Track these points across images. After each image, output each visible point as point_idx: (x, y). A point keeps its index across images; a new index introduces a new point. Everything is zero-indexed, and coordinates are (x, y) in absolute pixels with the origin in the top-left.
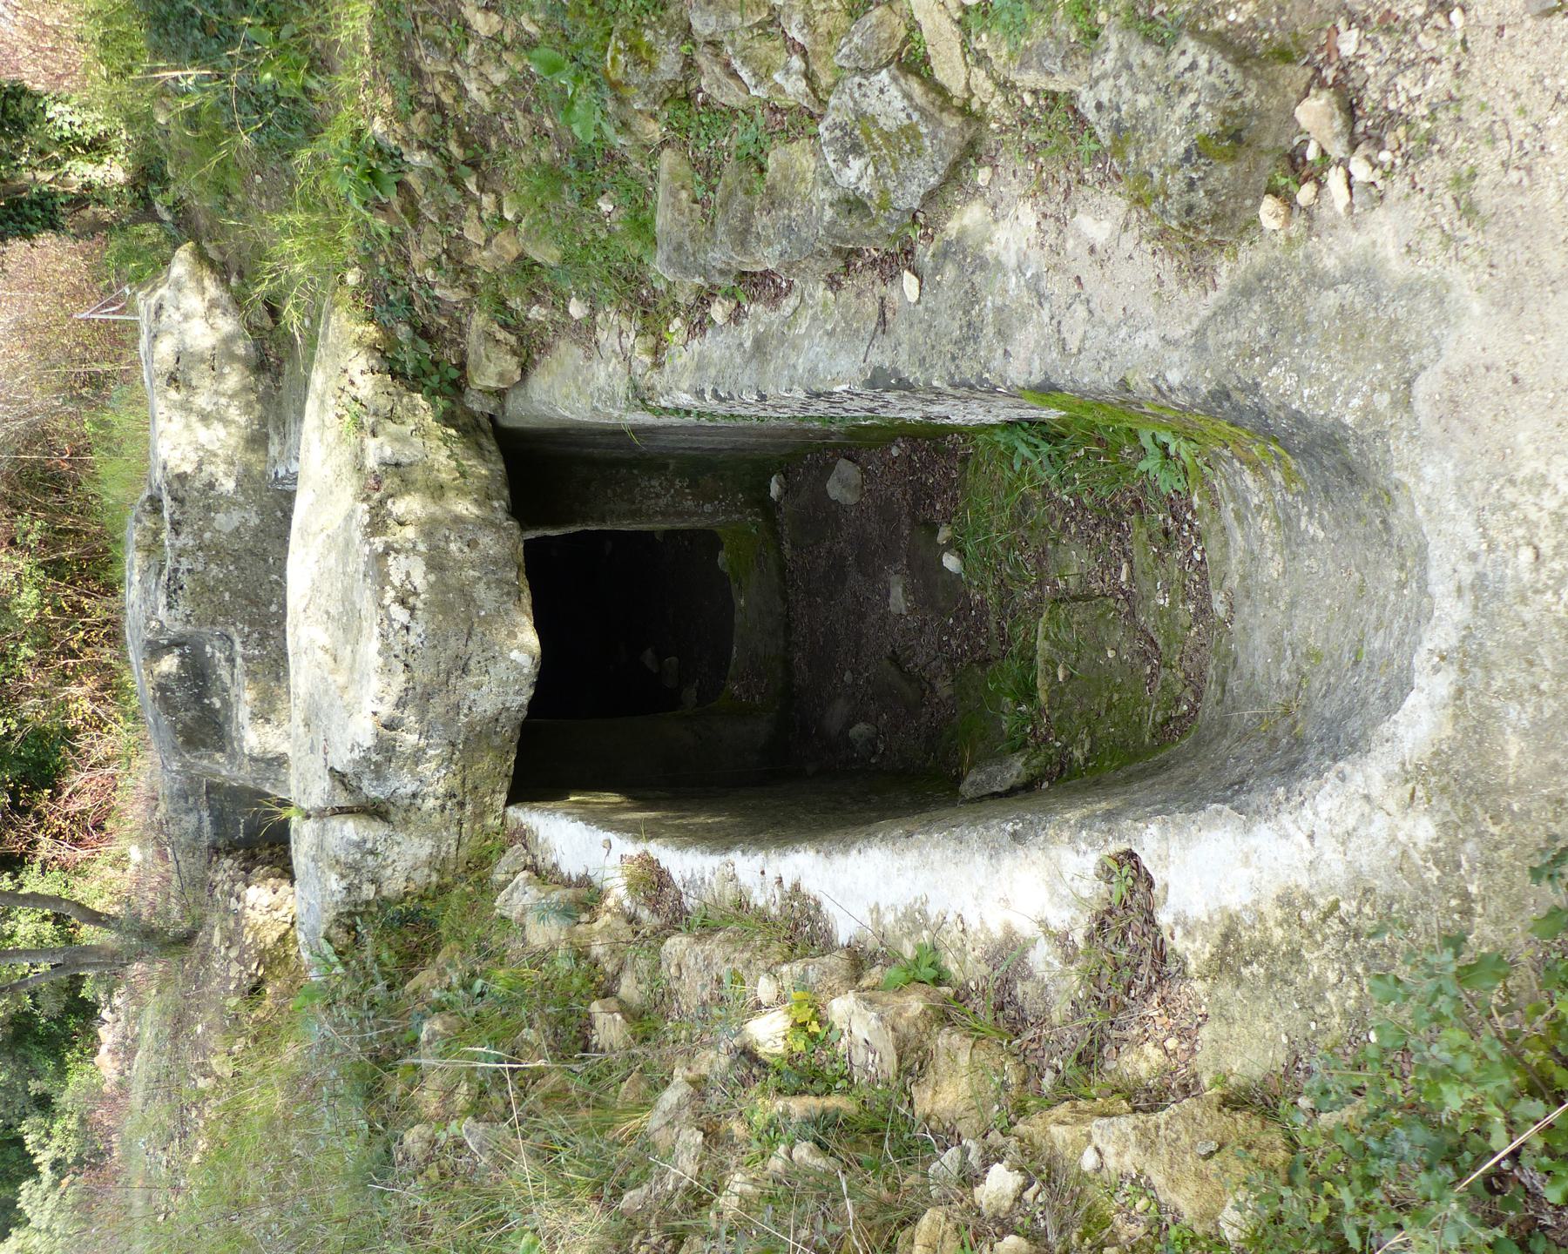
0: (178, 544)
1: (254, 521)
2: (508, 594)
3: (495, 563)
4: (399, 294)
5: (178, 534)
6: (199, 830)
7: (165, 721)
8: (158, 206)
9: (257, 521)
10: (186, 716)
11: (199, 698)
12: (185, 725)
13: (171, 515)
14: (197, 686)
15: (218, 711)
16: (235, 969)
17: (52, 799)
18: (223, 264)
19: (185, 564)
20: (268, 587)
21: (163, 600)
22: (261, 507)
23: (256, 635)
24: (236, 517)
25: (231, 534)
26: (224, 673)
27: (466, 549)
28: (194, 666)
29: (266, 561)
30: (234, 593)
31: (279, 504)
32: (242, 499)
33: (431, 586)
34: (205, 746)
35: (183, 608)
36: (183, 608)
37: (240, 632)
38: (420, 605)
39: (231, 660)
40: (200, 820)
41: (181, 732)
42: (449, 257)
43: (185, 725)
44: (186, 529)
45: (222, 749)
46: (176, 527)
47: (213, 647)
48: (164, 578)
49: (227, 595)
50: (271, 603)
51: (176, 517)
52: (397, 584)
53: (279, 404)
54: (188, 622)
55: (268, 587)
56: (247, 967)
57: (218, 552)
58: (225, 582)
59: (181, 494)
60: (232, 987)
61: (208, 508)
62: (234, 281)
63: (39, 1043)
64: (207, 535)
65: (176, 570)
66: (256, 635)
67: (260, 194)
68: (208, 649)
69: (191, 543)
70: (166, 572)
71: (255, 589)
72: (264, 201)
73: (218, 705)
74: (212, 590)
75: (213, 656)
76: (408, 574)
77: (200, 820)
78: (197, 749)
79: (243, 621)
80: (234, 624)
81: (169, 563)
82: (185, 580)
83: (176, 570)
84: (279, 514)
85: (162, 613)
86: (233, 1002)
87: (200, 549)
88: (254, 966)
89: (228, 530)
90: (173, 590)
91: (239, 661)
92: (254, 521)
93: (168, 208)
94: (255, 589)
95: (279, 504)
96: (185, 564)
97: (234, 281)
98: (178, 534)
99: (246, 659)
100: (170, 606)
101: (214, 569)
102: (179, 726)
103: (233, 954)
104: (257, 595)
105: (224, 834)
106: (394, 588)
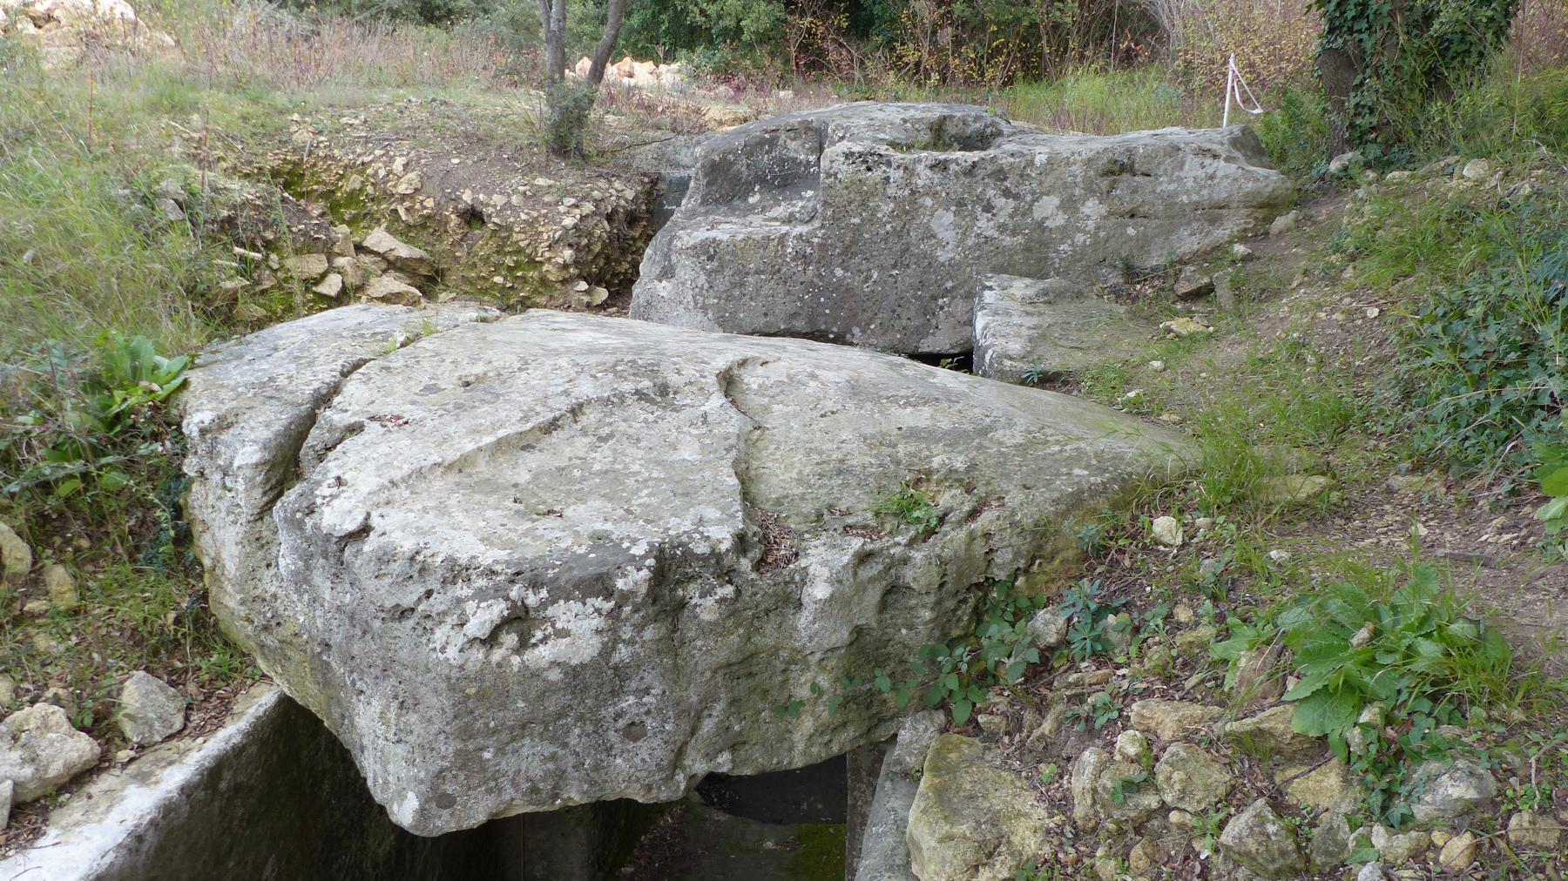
0: (920, 168)
1: (943, 256)
2: (534, 790)
3: (597, 768)
4: (1114, 637)
5: (932, 167)
6: (677, 165)
7: (739, 143)
8: (1350, 155)
9: (941, 259)
10: (741, 166)
11: (761, 180)
12: (731, 164)
13: (956, 161)
14: (774, 178)
15: (746, 200)
16: (498, 199)
17: (839, 28)
18: (1267, 234)
19: (896, 175)
20: (864, 267)
21: (857, 148)
22: (959, 265)
23: (809, 250)
24: (948, 235)
25: (928, 228)
26: (781, 210)
27: (621, 723)
28: (796, 176)
29: (894, 266)
30: (857, 229)
31: (961, 285)
32: (970, 242)
33: (536, 674)
34: (709, 184)
35: (845, 170)
36: (845, 170)
37: (813, 233)
38: (497, 655)
39: (790, 220)
40: (686, 167)
41: (724, 159)
42: (1151, 814)
43: (731, 164)
44: (937, 178)
45: (704, 202)
46: (940, 166)
47: (809, 200)
48: (883, 149)
49: (856, 221)
50: (846, 269)
51: (953, 167)
52: (550, 612)
53: (1079, 295)
54: (829, 176)
55: (864, 267)
56: (498, 214)
57: (907, 213)
58: (872, 219)
59: (980, 173)
60: (481, 197)
61: (960, 204)
62: (1240, 249)
63: (654, 16)
64: (928, 201)
65: (889, 164)
66: (809, 250)
67: (1349, 313)
68: (810, 193)
69: (920, 183)
70: (891, 151)
71: (861, 252)
72: (1338, 316)
73: (752, 200)
74: (863, 204)
75: (801, 198)
76: (562, 634)
77: (686, 167)
78: (705, 176)
79: (825, 238)
80: (823, 226)
81: (899, 155)
82: (877, 174)
83: (889, 164)
84: (949, 284)
85: (843, 146)
86: (467, 197)
87: (913, 192)
88: (496, 220)
89: (934, 226)
90: (868, 160)
91: (785, 229)
92: (943, 256)
93: (1346, 169)
94: (861, 252)
95: (961, 285)
96: (896, 175)
97: (1240, 249)
98: (932, 167)
99: (782, 239)
100: (848, 155)
101: (888, 207)
102: (731, 157)
103: (515, 200)
104: (855, 254)
105: (670, 190)
106: (544, 605)
